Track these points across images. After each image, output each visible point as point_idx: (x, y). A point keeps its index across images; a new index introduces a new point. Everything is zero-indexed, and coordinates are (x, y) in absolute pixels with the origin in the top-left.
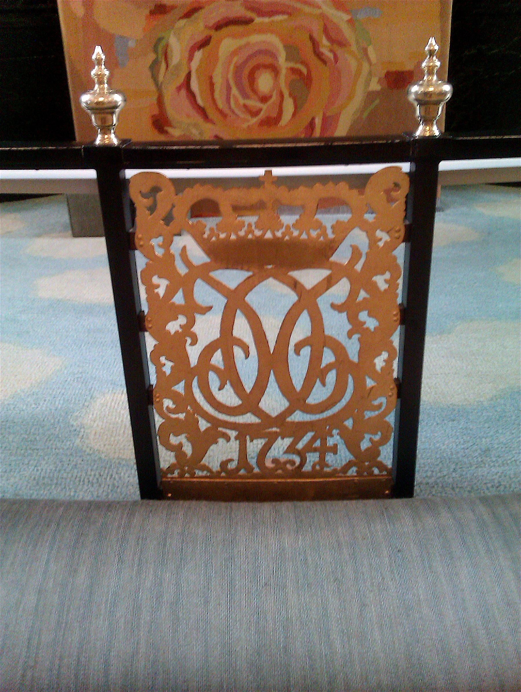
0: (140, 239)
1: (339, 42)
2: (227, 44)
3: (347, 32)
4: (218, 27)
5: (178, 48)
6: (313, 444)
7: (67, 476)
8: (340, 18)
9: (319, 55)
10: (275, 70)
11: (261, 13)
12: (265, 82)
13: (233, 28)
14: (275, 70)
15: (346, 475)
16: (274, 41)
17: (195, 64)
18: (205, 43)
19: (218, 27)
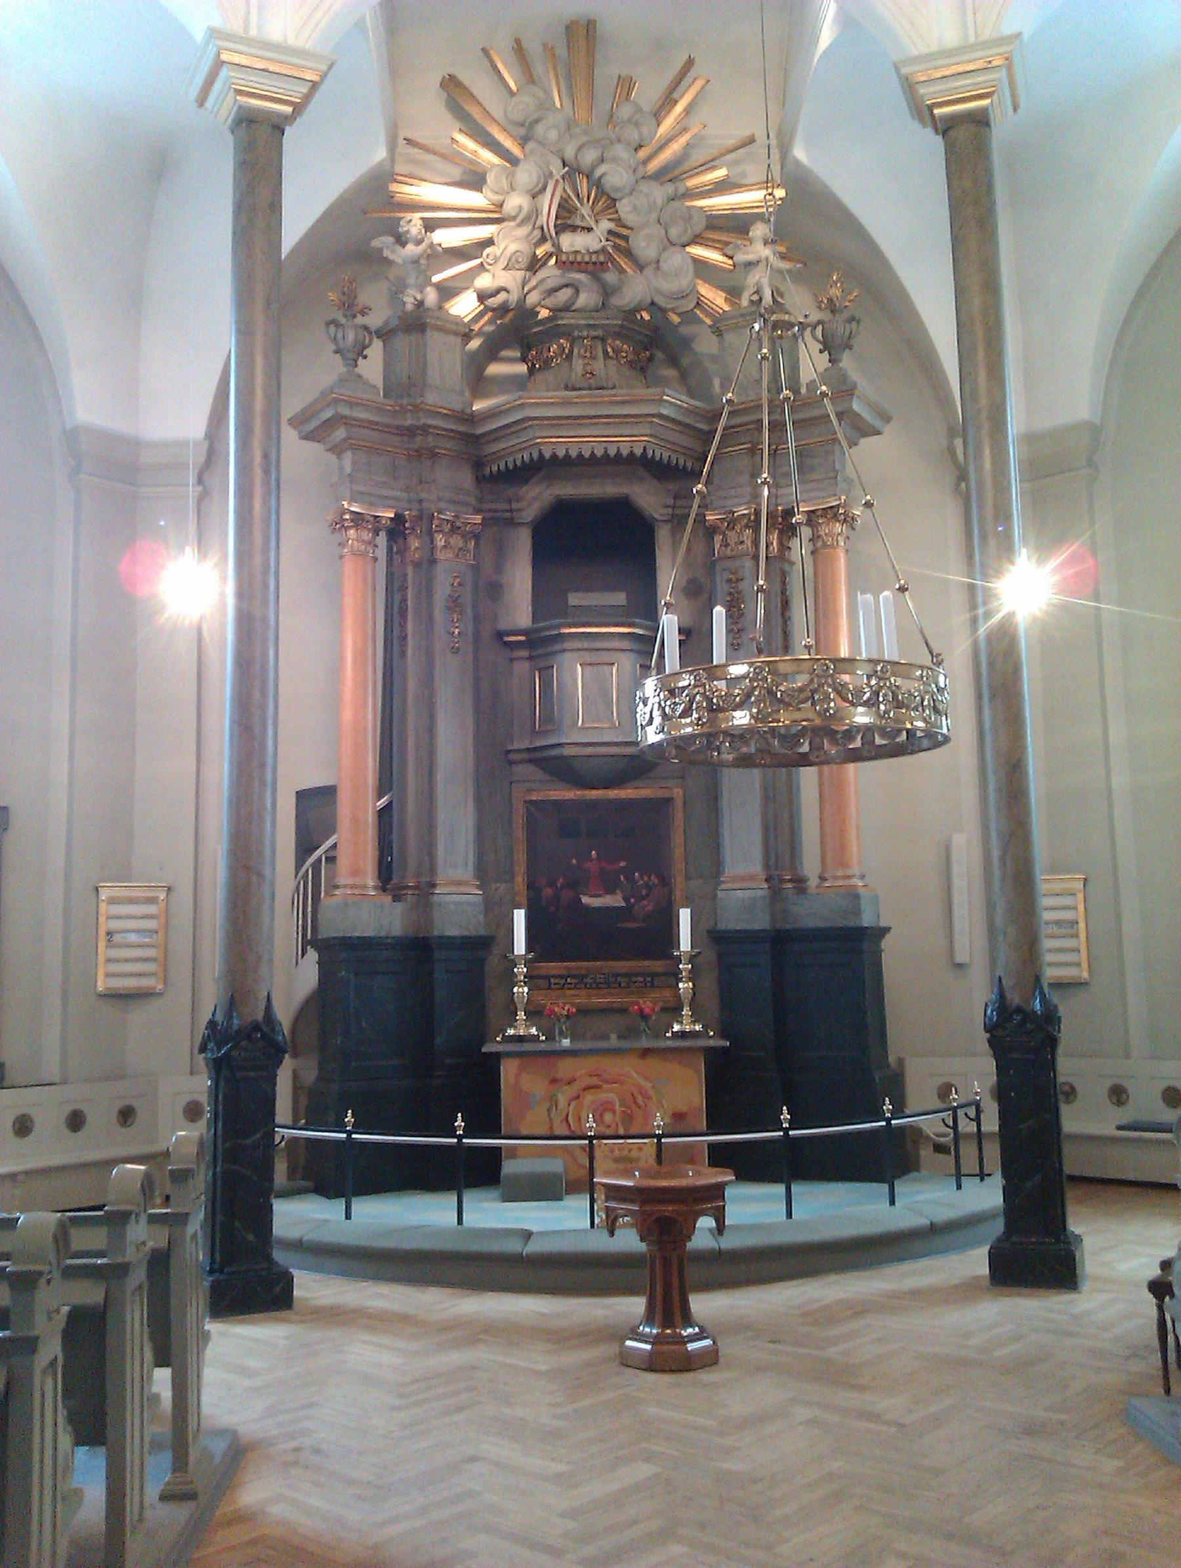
0: (192, 1112)
1: (647, 1097)
2: (589, 1098)
3: (652, 1093)
4: (584, 1090)
5: (562, 1099)
6: (722, 269)
7: (640, 134)
8: (647, 1085)
9: (635, 1102)
10: (614, 1112)
11: (607, 1082)
12: (608, 1117)
13: (592, 1091)
14: (614, 1112)
15: (289, 436)
16: (612, 1096)
17: (571, 1109)
18: (578, 1097)
19: (584, 1090)
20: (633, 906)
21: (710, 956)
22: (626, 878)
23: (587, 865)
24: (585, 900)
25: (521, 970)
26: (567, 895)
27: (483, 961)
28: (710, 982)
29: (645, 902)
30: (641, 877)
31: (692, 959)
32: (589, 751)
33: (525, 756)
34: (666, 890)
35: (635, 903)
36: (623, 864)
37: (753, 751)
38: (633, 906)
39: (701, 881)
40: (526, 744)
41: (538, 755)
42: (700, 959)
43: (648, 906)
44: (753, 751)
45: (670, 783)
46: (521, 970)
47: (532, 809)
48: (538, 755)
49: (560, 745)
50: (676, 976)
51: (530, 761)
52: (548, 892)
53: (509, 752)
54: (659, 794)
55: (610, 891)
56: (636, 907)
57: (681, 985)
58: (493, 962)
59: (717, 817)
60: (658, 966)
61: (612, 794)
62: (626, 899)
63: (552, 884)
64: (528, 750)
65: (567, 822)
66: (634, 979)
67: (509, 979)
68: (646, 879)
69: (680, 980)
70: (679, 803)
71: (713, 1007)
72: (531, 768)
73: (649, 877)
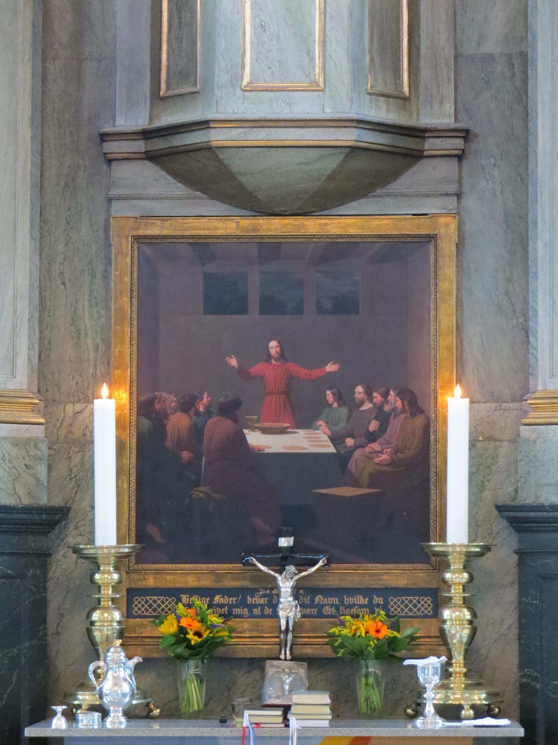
20: (350, 452)
21: (505, 555)
22: (340, 398)
23: (256, 369)
24: (255, 439)
25: (108, 576)
26: (218, 428)
27: (44, 557)
28: (503, 612)
29: (375, 446)
30: (369, 393)
31: (469, 560)
32: (261, 136)
33: (140, 146)
34: (419, 421)
35: (356, 447)
36: (331, 368)
37: (247, 713)
38: (350, 452)
39: (494, 405)
40: (141, 121)
41: (159, 144)
42: (486, 562)
43: (381, 454)
44: (247, 713)
45: (431, 206)
46: (108, 576)
47: (146, 249)
48: (159, 144)
49: (204, 124)
50: (437, 597)
51: (151, 157)
52: (178, 423)
53: (104, 137)
54: (409, 228)
55: (305, 422)
56: (357, 453)
57: (447, 614)
58: (63, 563)
59: (526, 273)
60: (396, 575)
61: (312, 226)
62: (335, 439)
63: (187, 405)
64: (146, 134)
65: (223, 283)
66: (348, 600)
67: (87, 595)
68: (377, 397)
69: (97, 605)
70: (448, 246)
71: (506, 661)
72: (149, 172)
73: (386, 395)
